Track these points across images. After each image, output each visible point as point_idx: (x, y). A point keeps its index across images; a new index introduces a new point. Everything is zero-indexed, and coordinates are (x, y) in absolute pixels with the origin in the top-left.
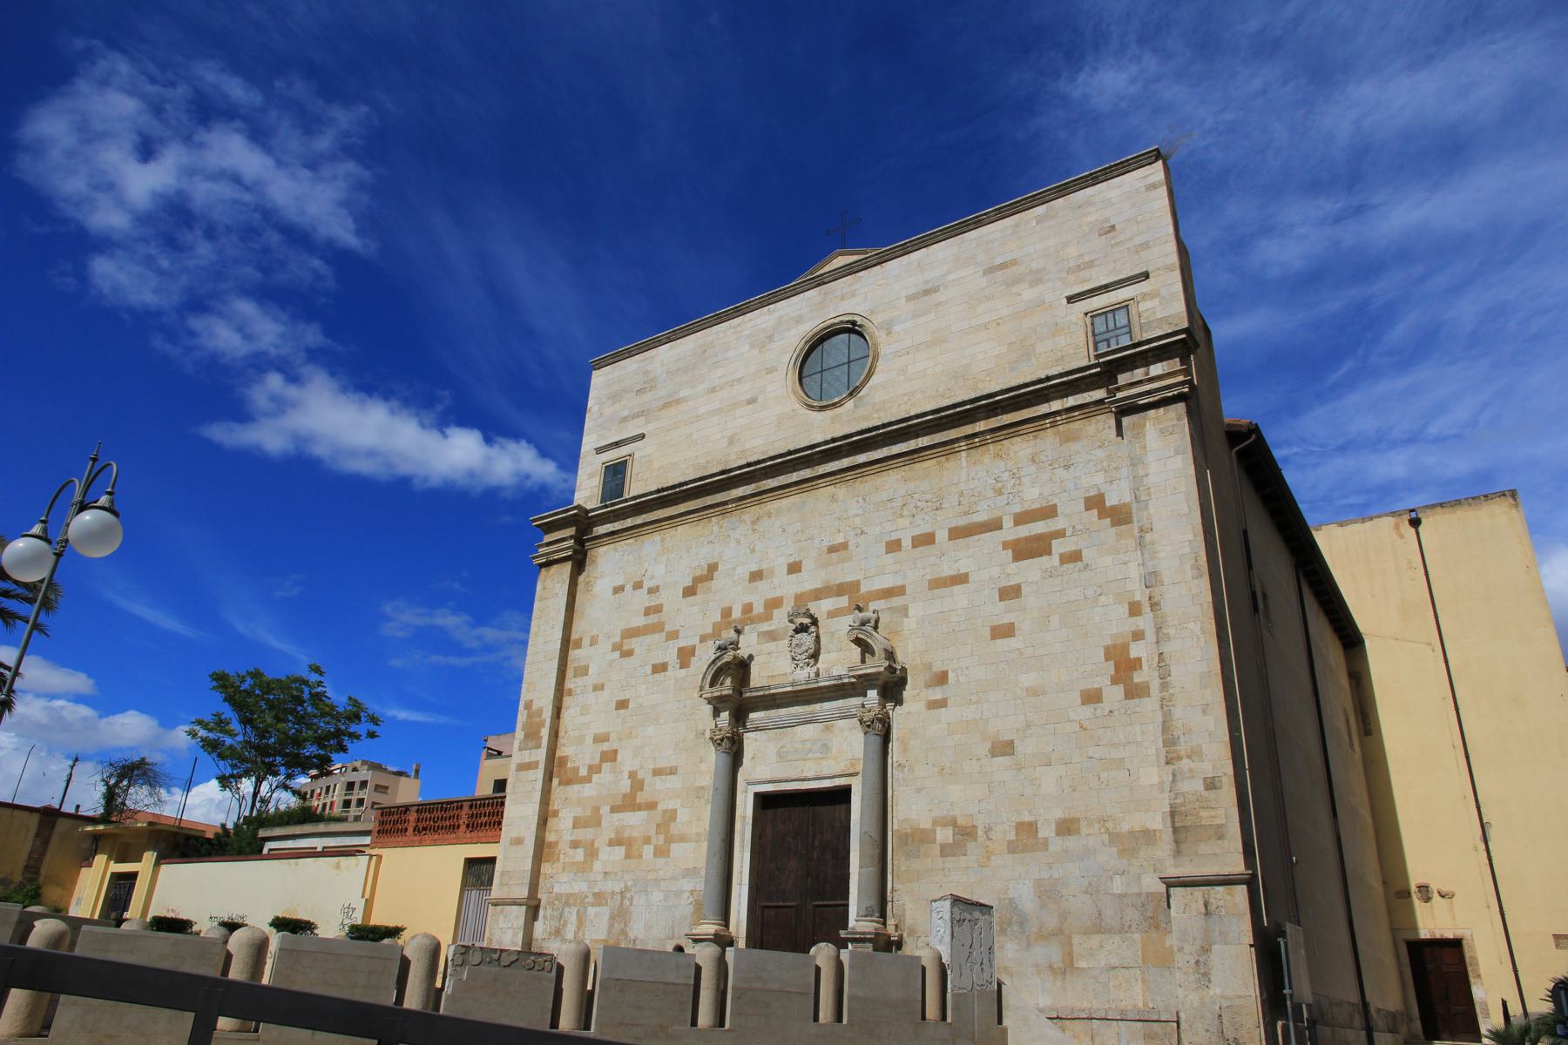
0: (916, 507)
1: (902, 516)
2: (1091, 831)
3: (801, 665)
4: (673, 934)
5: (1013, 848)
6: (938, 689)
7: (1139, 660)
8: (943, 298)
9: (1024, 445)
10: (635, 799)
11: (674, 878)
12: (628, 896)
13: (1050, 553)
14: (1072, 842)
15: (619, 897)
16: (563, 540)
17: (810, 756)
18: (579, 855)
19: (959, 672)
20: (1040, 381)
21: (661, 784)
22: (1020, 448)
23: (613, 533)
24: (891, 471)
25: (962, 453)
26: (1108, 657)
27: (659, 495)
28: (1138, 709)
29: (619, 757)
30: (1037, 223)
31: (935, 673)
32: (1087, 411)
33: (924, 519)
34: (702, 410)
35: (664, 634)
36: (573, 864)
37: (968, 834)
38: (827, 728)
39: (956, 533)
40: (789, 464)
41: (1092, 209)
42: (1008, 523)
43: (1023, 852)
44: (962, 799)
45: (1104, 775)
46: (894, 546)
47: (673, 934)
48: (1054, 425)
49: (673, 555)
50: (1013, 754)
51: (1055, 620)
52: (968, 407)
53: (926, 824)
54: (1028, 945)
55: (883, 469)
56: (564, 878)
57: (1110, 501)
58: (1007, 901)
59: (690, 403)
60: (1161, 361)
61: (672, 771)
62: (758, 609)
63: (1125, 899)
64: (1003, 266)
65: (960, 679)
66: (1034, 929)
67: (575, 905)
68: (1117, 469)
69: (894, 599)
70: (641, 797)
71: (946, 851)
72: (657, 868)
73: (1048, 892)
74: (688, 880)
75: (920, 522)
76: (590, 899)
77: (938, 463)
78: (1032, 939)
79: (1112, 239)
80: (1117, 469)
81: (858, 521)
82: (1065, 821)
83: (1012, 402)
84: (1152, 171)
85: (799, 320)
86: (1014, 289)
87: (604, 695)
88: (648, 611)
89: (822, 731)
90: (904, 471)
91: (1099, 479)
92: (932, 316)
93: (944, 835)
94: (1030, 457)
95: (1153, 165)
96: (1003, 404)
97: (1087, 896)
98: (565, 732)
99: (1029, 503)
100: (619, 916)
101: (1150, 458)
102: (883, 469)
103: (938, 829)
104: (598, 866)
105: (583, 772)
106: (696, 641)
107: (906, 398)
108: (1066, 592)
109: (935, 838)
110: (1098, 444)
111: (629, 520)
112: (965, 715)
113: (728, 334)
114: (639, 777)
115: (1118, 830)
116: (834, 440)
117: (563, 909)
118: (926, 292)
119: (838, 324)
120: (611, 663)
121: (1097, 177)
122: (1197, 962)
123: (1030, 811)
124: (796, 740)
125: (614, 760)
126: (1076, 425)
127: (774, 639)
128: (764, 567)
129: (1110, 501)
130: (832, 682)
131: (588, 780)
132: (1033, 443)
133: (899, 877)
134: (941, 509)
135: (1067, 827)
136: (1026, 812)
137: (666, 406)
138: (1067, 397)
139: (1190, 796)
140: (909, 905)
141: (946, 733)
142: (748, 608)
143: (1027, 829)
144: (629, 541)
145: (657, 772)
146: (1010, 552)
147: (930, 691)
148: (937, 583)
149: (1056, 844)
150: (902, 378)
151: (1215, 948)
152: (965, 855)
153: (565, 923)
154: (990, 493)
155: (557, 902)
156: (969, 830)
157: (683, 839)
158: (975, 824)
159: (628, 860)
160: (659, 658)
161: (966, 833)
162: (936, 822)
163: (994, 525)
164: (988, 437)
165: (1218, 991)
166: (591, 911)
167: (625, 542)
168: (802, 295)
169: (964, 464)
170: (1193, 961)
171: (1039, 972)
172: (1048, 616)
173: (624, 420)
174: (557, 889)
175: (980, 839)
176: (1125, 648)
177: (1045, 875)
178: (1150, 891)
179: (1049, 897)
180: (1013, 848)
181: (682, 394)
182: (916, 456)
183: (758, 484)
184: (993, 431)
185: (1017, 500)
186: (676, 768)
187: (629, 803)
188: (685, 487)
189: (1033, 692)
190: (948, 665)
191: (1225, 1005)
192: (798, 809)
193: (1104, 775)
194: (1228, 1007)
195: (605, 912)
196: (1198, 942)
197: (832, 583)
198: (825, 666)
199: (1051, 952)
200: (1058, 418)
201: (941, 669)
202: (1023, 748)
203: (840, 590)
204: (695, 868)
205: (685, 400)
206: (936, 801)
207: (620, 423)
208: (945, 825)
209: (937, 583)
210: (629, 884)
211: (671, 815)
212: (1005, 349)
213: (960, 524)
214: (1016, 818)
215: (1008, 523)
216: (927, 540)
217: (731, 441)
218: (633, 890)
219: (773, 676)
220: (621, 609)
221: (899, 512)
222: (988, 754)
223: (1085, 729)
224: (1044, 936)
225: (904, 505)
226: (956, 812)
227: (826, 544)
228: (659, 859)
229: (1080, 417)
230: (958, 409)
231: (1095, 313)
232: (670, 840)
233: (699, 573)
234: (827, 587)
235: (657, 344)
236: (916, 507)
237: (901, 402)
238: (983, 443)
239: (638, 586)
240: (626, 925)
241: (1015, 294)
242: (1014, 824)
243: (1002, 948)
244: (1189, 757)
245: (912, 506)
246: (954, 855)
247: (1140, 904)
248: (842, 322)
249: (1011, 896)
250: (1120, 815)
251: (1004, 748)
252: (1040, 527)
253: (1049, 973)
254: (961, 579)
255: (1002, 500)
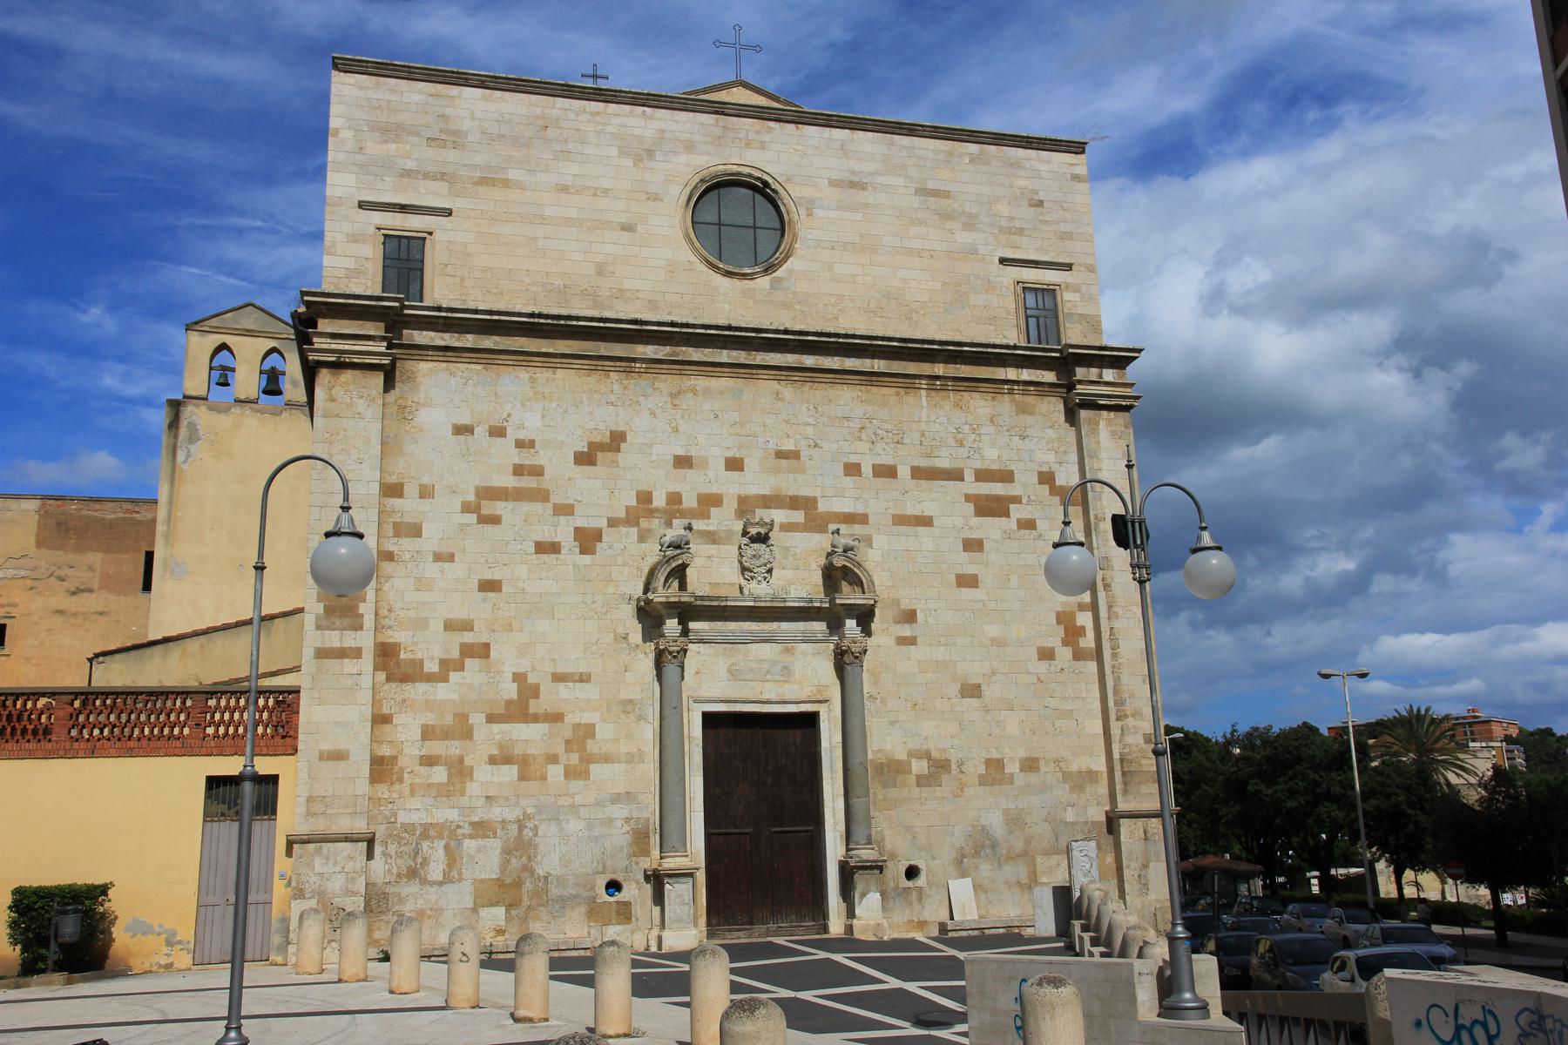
0: (875, 434)
1: (860, 439)
2: (1048, 770)
3: (759, 578)
4: (604, 867)
5: (983, 781)
6: (907, 626)
7: (1083, 628)
8: (871, 200)
9: (983, 403)
10: (527, 707)
11: (599, 804)
12: (530, 825)
13: (1008, 516)
14: (1032, 778)
15: (515, 827)
16: (334, 336)
17: (769, 677)
18: (440, 774)
19: (928, 613)
20: (1007, 347)
21: (565, 691)
22: (980, 405)
23: (447, 349)
24: (846, 386)
25: (922, 391)
26: (1059, 621)
27: (532, 320)
28: (1083, 670)
29: (493, 654)
30: (970, 161)
31: (903, 610)
32: (1041, 389)
33: (884, 450)
34: (550, 211)
35: (549, 506)
36: (429, 785)
37: (942, 767)
38: (787, 649)
39: (919, 473)
40: (722, 339)
41: (1022, 173)
42: (969, 476)
43: (992, 785)
44: (936, 734)
45: (1058, 723)
46: (853, 469)
47: (604, 867)
48: (1011, 392)
49: (554, 405)
50: (980, 697)
51: (1014, 579)
52: (936, 347)
53: (903, 757)
54: (1000, 865)
55: (837, 381)
56: (416, 803)
57: (1060, 482)
58: (980, 828)
59: (527, 193)
60: (1113, 368)
61: (583, 678)
62: (689, 501)
63: (1076, 827)
64: (936, 193)
65: (929, 620)
66: (1004, 852)
67: (441, 837)
68: (1065, 452)
69: (857, 526)
70: (534, 706)
71: (921, 781)
72: (571, 792)
73: (1015, 821)
74: (619, 806)
75: (881, 452)
76: (467, 830)
77: (898, 394)
78: (1003, 859)
79: (1041, 214)
80: (1065, 452)
81: (810, 431)
82: (1028, 759)
83: (975, 355)
84: (1076, 161)
85: (690, 147)
86: (948, 225)
87: (455, 570)
88: (518, 470)
89: (782, 653)
90: (860, 390)
91: (1051, 457)
92: (859, 216)
93: (920, 767)
94: (990, 417)
95: (1079, 156)
96: (965, 355)
97: (1047, 824)
98: (390, 611)
99: (989, 462)
100: (517, 850)
101: (1103, 455)
102: (837, 381)
103: (913, 760)
104: (473, 788)
105: (432, 667)
106: (603, 523)
107: (833, 301)
108: (1024, 555)
109: (911, 770)
110: (1050, 424)
111: (470, 337)
112: (934, 654)
113: (580, 118)
114: (529, 681)
115: (1069, 770)
116: (786, 332)
117: (417, 844)
118: (853, 185)
119: (744, 175)
120: (462, 527)
121: (1031, 143)
122: (1139, 876)
123: (997, 749)
124: (751, 658)
125: (487, 655)
126: (1031, 399)
127: (714, 542)
128: (693, 453)
129: (1060, 482)
130: (802, 604)
131: (442, 677)
132: (992, 403)
133: (875, 805)
134: (902, 443)
135: (1030, 765)
136: (993, 750)
137: (483, 181)
138: (1022, 368)
139: (1135, 748)
140: (887, 832)
141: (917, 670)
142: (675, 499)
143: (995, 765)
144: (472, 366)
145: (558, 678)
146: (972, 505)
147: (899, 627)
148: (901, 520)
149: (1020, 779)
150: (827, 274)
151: (1152, 864)
152: (940, 786)
153: (425, 862)
154: (952, 442)
155: (405, 835)
156: (942, 763)
157: (607, 759)
158: (948, 758)
159: (524, 783)
160: (546, 535)
161: (939, 767)
162: (911, 754)
163: (955, 475)
164: (949, 383)
165: (1154, 897)
166: (470, 845)
167: (467, 365)
168: (692, 114)
169: (925, 404)
170: (1136, 875)
171: (1010, 888)
172: (1008, 575)
173: (408, 174)
174: (403, 818)
175: (954, 772)
176: (1072, 616)
177: (1011, 805)
178: (1095, 820)
179: (1015, 824)
180: (983, 781)
181: (514, 174)
182: (874, 378)
183: (674, 348)
184: (955, 379)
185: (977, 456)
186: (589, 675)
187: (518, 710)
188: (574, 323)
189: (997, 643)
190: (916, 604)
191: (1158, 906)
192: (744, 731)
193: (1058, 723)
194: (1161, 908)
195: (494, 847)
196: (1140, 861)
197: (783, 493)
198: (780, 582)
199: (1019, 871)
200: (1016, 387)
201: (909, 607)
202: (990, 692)
203: (794, 503)
204: (628, 793)
205: (521, 186)
206: (910, 735)
207: (401, 175)
208: (919, 758)
209: (901, 520)
210: (529, 811)
211: (589, 731)
212: (938, 286)
213: (922, 464)
214: (985, 755)
215: (969, 476)
216: (886, 472)
217: (601, 270)
218: (537, 817)
219: (716, 584)
220: (471, 458)
221: (857, 434)
222: (958, 694)
223: (1042, 682)
224: (1011, 857)
225: (863, 428)
226: (931, 746)
227: (772, 446)
228: (573, 782)
229: (1034, 393)
230: (926, 346)
231: (1029, 285)
232: (588, 759)
233: (597, 438)
234: (777, 496)
235: (463, 82)
236: (875, 434)
237: (827, 303)
238: (944, 387)
239: (498, 432)
240: (529, 859)
241: (949, 230)
242: (983, 760)
243: (977, 868)
244: (1133, 716)
245: (870, 432)
246: (930, 786)
247: (1087, 831)
248: (750, 176)
249: (983, 823)
250: (1071, 758)
251: (972, 691)
252: (998, 489)
253: (1018, 888)
254: (926, 521)
255: (963, 452)
